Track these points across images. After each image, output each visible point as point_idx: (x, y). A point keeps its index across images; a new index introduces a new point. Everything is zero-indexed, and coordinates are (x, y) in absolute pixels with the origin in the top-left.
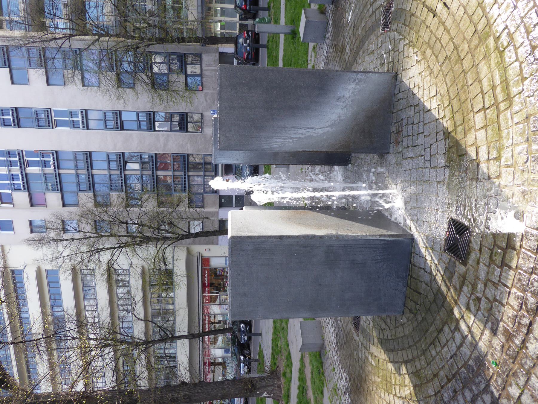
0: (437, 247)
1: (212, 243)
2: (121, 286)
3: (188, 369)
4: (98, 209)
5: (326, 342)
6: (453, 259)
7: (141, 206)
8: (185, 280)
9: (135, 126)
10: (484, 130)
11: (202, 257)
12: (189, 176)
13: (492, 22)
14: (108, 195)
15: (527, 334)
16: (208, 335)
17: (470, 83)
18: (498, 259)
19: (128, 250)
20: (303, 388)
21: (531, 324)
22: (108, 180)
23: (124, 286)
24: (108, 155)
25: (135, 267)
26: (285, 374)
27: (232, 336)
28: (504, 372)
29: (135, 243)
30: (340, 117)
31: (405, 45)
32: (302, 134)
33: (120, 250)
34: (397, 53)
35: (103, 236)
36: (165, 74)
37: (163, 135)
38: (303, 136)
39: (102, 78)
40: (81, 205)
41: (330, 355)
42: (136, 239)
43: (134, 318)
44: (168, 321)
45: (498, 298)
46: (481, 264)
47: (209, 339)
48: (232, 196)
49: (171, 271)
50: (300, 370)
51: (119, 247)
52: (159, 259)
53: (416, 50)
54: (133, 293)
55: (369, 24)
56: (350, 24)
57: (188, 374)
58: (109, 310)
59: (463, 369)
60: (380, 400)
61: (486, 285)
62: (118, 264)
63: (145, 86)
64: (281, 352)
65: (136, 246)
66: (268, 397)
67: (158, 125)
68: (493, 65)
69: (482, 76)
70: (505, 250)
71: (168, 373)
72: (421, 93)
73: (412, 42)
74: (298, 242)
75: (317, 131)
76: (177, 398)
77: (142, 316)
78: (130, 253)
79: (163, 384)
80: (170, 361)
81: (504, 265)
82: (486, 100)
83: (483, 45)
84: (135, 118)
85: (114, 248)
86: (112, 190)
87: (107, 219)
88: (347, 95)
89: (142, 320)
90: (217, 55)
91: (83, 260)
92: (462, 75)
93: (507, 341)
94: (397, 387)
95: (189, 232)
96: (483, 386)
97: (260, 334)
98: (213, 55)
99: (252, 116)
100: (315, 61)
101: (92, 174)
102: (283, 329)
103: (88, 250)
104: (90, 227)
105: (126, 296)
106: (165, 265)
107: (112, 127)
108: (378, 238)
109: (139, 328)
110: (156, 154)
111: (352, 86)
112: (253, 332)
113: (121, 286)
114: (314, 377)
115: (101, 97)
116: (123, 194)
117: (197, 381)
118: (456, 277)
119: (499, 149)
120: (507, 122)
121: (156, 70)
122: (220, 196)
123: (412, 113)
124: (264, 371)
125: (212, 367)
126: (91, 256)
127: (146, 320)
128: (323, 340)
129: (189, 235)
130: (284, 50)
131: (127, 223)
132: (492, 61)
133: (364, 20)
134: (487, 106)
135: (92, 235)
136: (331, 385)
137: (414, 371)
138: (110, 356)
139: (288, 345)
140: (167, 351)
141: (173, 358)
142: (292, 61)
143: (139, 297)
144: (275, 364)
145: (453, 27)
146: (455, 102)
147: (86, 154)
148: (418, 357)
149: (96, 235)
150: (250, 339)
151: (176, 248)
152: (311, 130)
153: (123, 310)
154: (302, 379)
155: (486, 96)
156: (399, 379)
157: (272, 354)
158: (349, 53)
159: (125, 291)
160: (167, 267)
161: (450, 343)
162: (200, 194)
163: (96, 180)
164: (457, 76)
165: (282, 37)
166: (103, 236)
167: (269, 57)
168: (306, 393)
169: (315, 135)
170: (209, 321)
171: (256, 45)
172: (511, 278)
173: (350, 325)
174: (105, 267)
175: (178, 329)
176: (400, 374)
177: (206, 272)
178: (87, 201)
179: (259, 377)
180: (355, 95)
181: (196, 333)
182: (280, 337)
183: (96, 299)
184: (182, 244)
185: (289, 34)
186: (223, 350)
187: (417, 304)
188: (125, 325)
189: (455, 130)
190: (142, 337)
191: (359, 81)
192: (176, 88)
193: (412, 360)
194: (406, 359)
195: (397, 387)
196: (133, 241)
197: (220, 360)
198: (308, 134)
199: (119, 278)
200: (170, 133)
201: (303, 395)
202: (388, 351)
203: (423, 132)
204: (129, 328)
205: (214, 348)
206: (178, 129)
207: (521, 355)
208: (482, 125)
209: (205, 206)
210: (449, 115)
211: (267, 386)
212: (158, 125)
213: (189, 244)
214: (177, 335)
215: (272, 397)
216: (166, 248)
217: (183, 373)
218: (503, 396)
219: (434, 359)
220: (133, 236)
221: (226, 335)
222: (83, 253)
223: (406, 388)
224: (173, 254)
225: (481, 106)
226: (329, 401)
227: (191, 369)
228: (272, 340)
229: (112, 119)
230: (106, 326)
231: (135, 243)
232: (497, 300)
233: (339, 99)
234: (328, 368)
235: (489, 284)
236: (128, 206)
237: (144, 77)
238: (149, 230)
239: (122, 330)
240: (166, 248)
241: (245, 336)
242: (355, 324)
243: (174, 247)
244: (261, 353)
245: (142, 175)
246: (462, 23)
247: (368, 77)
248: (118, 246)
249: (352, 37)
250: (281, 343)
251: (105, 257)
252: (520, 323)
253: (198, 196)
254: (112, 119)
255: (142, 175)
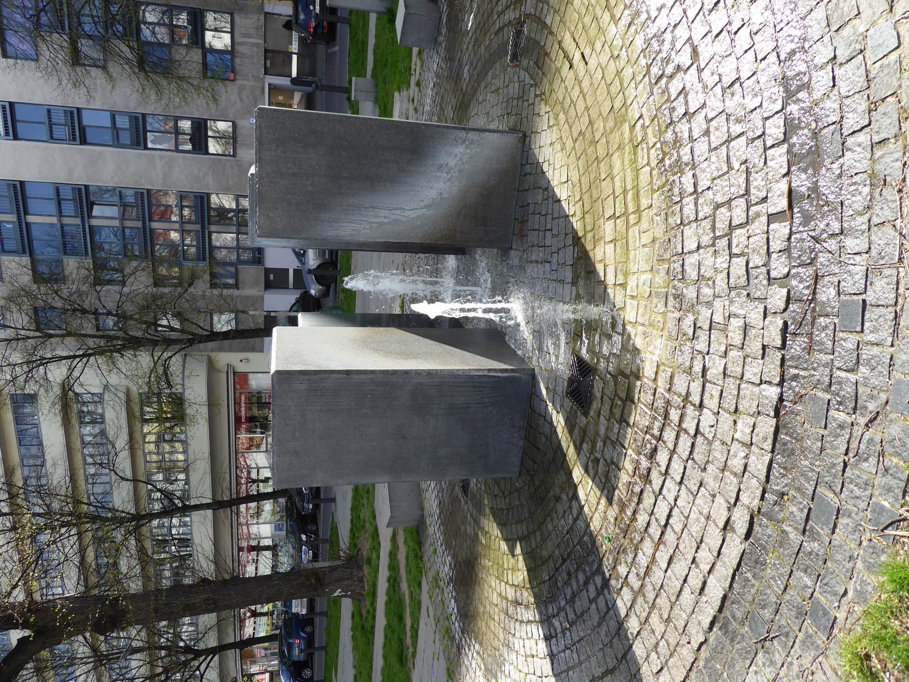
0: (559, 389)
1: (253, 350)
2: (88, 423)
3: (211, 557)
4: (42, 288)
5: (426, 513)
6: (575, 407)
7: (123, 283)
8: (204, 410)
9: (108, 137)
10: (613, 245)
11: (234, 373)
12: (210, 234)
13: (629, 102)
14: (60, 262)
15: (638, 504)
16: (247, 503)
17: (603, 177)
18: (617, 412)
19: (100, 361)
20: (395, 579)
21: (642, 492)
22: (59, 233)
23: (93, 422)
24: (57, 189)
25: (113, 390)
26: (369, 561)
27: (287, 503)
28: (615, 549)
29: (112, 348)
30: (441, 194)
31: (536, 96)
32: (385, 217)
33: (85, 360)
34: (526, 103)
35: (51, 336)
36: (163, 45)
37: (161, 158)
38: (386, 221)
39: (43, 47)
40: (8, 280)
41: (431, 530)
42: (114, 342)
43: (114, 477)
44: (176, 480)
45: (615, 460)
46: (602, 417)
47: (247, 509)
48: (287, 270)
49: (179, 395)
50: (391, 553)
51: (83, 356)
52: (157, 376)
53: (548, 109)
54: (111, 433)
55: (495, 45)
56: (470, 34)
57: (213, 567)
58: (67, 464)
59: (578, 547)
60: (490, 590)
61: (605, 443)
62: (82, 385)
63: (126, 67)
64: (364, 527)
65: (115, 354)
66: (343, 596)
67: (153, 138)
68: (626, 162)
69: (615, 172)
70: (624, 402)
71: (177, 567)
72: (551, 172)
73: (544, 93)
74: (373, 379)
75: (407, 213)
76: (194, 604)
77: (129, 474)
78: (103, 367)
79: (166, 583)
80: (180, 547)
81: (624, 421)
82: (617, 206)
83: (618, 130)
84: (108, 123)
85: (74, 357)
86: (65, 253)
87: (59, 304)
88: (452, 162)
89: (127, 480)
90: (262, 17)
91: (15, 379)
92: (595, 164)
93: (620, 511)
94: (510, 572)
95: (212, 331)
96: (595, 567)
97: (333, 500)
98: (256, 17)
99: (310, 188)
100: (420, 74)
101: (27, 223)
102: (368, 492)
103: (25, 360)
104: (26, 319)
105: (98, 440)
106: (170, 386)
107: (63, 137)
108: (486, 373)
109: (124, 494)
110: (148, 191)
111: (460, 150)
112: (322, 497)
113: (88, 423)
114: (410, 563)
115: (41, 82)
116: (89, 262)
117: (227, 577)
118: (576, 431)
119: (626, 274)
120: (635, 241)
121: (146, 32)
122: (266, 269)
123: (539, 198)
124: (339, 558)
125: (254, 553)
126: (29, 372)
127: (135, 480)
128: (422, 509)
129: (214, 336)
130: (376, 35)
131: (96, 313)
132: (626, 155)
133: (488, 35)
134: (617, 214)
135: (31, 334)
136: (431, 574)
137: (529, 550)
138: (72, 543)
139: (374, 517)
140: (174, 531)
141: (185, 542)
142: (387, 60)
143: (121, 442)
144: (355, 546)
145: (590, 93)
146: (586, 197)
147: (15, 186)
148: (534, 532)
149: (38, 334)
150: (316, 507)
151: (188, 359)
152: (398, 212)
153: (95, 464)
154: (393, 567)
155: (617, 200)
156: (512, 561)
157: (351, 530)
158: (467, 80)
159: (97, 430)
160: (174, 390)
161: (567, 514)
162: (231, 264)
163: (35, 233)
164: (590, 163)
165: (373, 18)
166: (51, 336)
167: (351, 40)
168: (399, 586)
169: (404, 219)
170: (248, 477)
171: (332, 18)
172: (629, 436)
173: (457, 488)
174: (57, 390)
175: (193, 493)
176: (513, 556)
177: (243, 398)
178: (18, 272)
179: (329, 567)
180: (463, 163)
181: (226, 499)
182: (363, 505)
183: (41, 444)
184: (199, 350)
185: (384, 13)
186: (273, 525)
187: (535, 462)
188: (98, 489)
189: (584, 235)
190: (129, 508)
191: (470, 144)
192: (186, 72)
193: (526, 537)
194: (520, 535)
195: (510, 572)
196: (109, 344)
197: (268, 542)
198: (394, 217)
199: (85, 409)
200: (175, 154)
201: (395, 590)
202: (502, 525)
203: (551, 230)
204: (106, 494)
205: (257, 523)
206: (189, 147)
207: (631, 529)
208: (612, 238)
209: (241, 285)
210: (579, 214)
211: (340, 580)
212: (153, 138)
213: (212, 351)
214: (193, 503)
215: (349, 597)
216: (171, 357)
217: (204, 565)
218: (613, 577)
219: (550, 534)
220: (110, 337)
221: (277, 502)
222: (15, 365)
223: (520, 573)
224: (184, 367)
225: (612, 212)
226: (428, 596)
227: (217, 559)
228: (352, 509)
229: (63, 122)
230: (63, 492)
231: (112, 348)
232: (613, 463)
233: (440, 168)
234: (428, 550)
235: (608, 442)
236: (98, 282)
237: (125, 49)
238: (139, 326)
239: (92, 498)
240: (171, 357)
241: (308, 503)
242: (463, 487)
243: (186, 355)
244: (334, 529)
245: (124, 228)
246: (599, 90)
247: (483, 138)
248: (81, 352)
249: (472, 55)
250: (365, 513)
251: (57, 373)
252: (632, 491)
253: (229, 268)
254: (63, 122)
255: (124, 228)
